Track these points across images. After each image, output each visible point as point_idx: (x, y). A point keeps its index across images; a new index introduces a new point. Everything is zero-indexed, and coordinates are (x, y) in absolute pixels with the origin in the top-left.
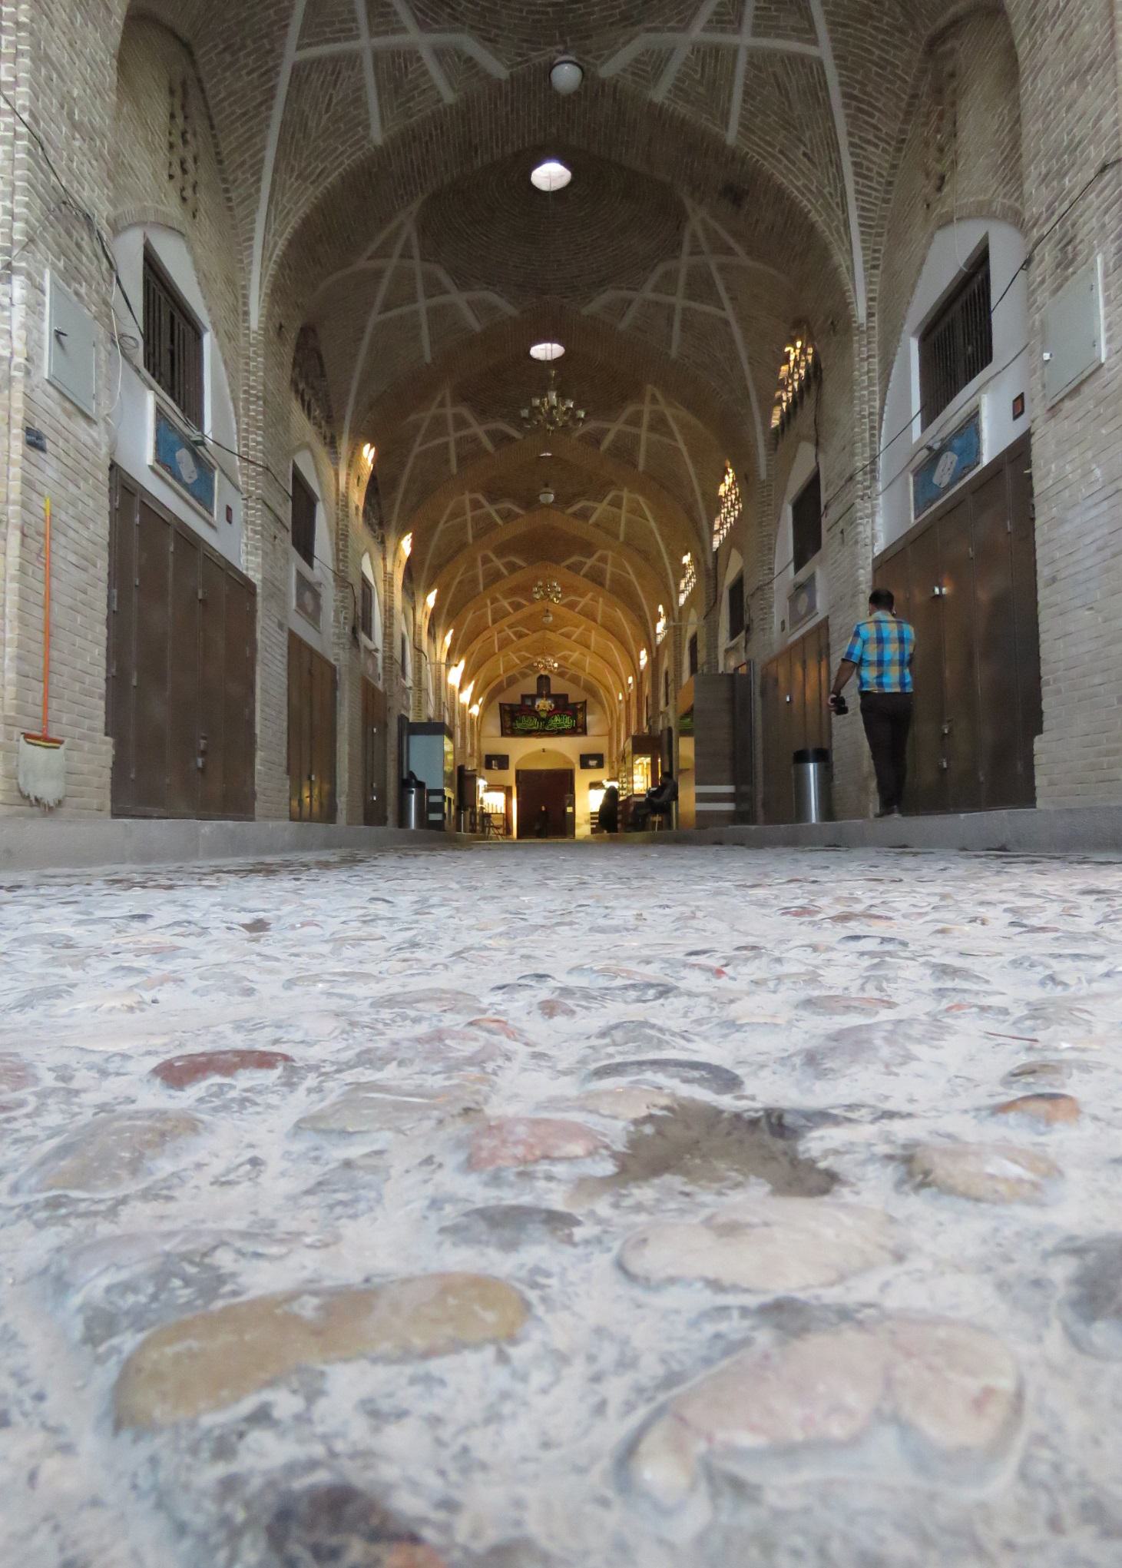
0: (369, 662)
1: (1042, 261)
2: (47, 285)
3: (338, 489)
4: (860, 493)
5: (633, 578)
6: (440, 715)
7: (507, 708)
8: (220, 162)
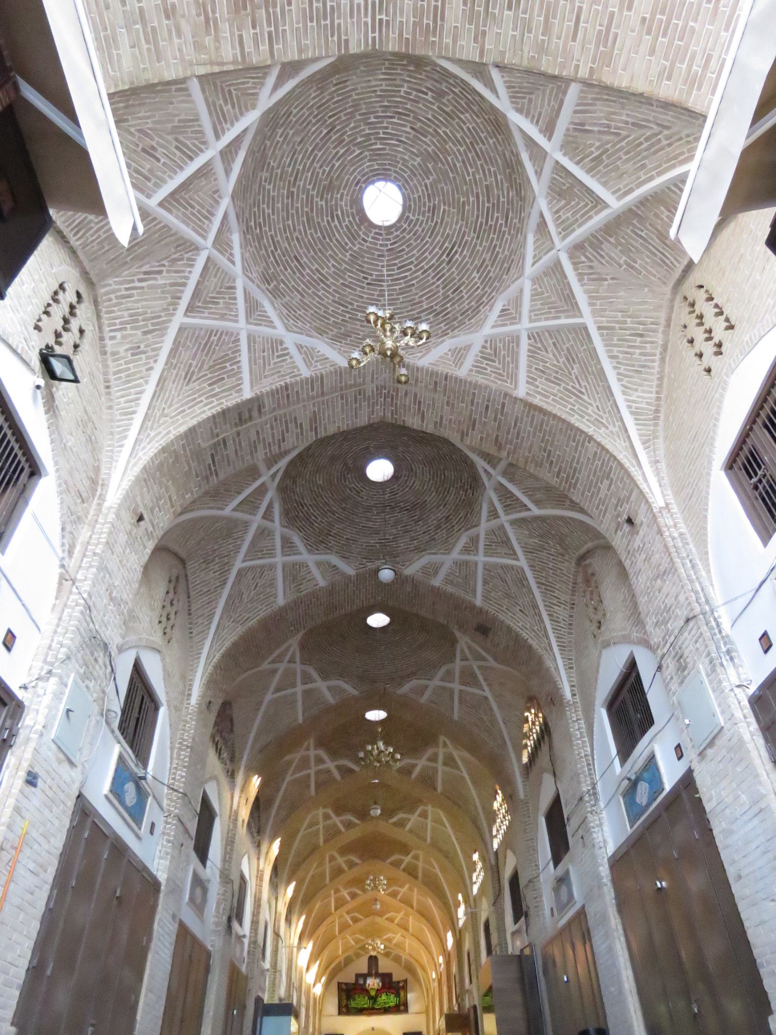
0: (238, 947)
1: (668, 667)
2: (70, 682)
3: (231, 808)
4: (589, 809)
5: (438, 871)
6: (289, 996)
7: (344, 987)
8: (190, 614)
